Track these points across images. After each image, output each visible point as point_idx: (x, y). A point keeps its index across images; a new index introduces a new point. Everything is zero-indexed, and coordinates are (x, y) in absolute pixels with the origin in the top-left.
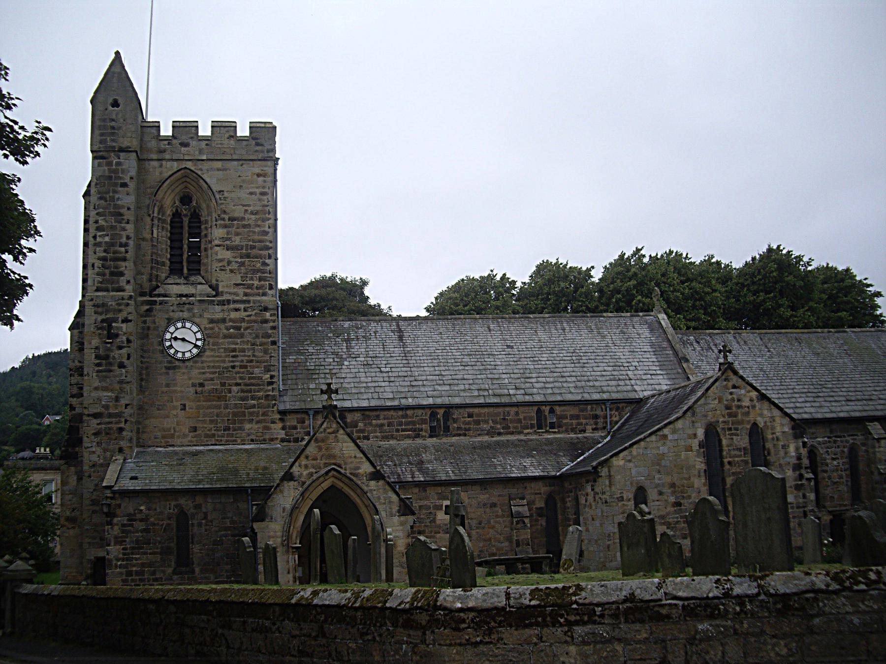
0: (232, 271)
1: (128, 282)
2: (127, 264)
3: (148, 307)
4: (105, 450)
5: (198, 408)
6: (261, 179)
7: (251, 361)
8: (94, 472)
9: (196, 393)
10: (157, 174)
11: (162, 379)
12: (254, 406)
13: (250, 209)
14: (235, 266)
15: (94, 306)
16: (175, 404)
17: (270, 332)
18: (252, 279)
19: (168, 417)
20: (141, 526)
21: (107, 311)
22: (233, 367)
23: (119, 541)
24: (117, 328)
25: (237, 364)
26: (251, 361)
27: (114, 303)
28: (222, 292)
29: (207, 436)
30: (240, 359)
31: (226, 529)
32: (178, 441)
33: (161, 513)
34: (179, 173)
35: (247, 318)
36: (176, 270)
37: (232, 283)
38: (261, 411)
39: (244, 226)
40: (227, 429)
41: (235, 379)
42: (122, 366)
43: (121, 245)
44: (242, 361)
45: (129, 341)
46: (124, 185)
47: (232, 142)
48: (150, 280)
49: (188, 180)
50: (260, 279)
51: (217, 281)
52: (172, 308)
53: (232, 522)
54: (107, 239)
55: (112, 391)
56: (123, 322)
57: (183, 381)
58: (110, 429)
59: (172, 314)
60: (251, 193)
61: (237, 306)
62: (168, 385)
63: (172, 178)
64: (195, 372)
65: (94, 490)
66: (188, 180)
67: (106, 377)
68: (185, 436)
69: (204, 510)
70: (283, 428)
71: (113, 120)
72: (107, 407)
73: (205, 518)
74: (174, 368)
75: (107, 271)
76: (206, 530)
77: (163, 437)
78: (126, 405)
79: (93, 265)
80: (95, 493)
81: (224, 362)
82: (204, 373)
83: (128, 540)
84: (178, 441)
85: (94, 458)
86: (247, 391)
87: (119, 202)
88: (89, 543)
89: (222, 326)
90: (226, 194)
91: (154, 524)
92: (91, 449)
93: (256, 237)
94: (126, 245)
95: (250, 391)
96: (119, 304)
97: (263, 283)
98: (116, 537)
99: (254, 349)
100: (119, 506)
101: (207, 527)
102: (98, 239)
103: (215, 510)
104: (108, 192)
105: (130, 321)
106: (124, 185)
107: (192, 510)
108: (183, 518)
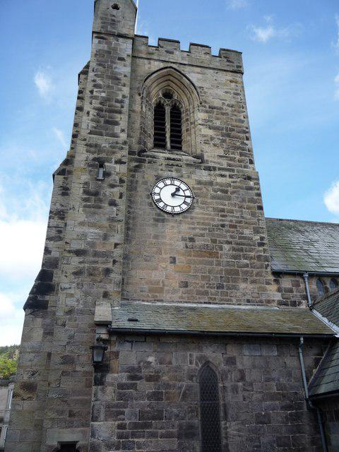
0: (215, 145)
1: (123, 131)
2: (122, 116)
3: (136, 164)
4: (87, 294)
5: (189, 262)
6: (233, 85)
7: (240, 222)
8: (70, 320)
9: (187, 247)
10: (147, 68)
11: (150, 231)
12: (247, 266)
13: (226, 103)
14: (218, 142)
15: (86, 145)
16: (164, 256)
17: (255, 198)
18: (233, 153)
19: (156, 269)
20: (146, 387)
21: (100, 151)
22: (223, 226)
23: (114, 412)
24: (110, 167)
25: (227, 223)
26: (240, 222)
27: (107, 146)
28: (207, 161)
29: (199, 293)
30: (229, 219)
31: (273, 397)
32: (168, 297)
33: (178, 368)
34: (166, 70)
35: (232, 184)
36: (159, 143)
37: (216, 154)
38: (255, 271)
39: (223, 114)
40: (220, 287)
41: (225, 237)
42: (113, 203)
43: (117, 101)
44: (231, 221)
45: (122, 181)
46: (122, 59)
47: (208, 56)
48: (139, 143)
49: (172, 78)
50: (241, 155)
51: (202, 151)
52: (161, 167)
53: (280, 387)
54: (103, 95)
55: (100, 227)
56: (116, 162)
57: (173, 235)
58: (94, 269)
59: (160, 172)
60: (226, 92)
61: (223, 173)
62: (156, 237)
63: (158, 73)
64: (184, 227)
65: (68, 343)
66: (172, 78)
67: (95, 213)
68: (174, 291)
69: (239, 366)
70: (279, 290)
71: (114, 16)
72: (92, 244)
73: (242, 378)
74: (163, 221)
75: (102, 120)
76: (244, 399)
77: (150, 291)
78: (116, 245)
79: (88, 113)
80: (68, 348)
81: (214, 220)
82: (193, 229)
83: (126, 410)
84: (168, 297)
85: (71, 302)
86: (238, 250)
87: (117, 70)
88: (52, 419)
89: (210, 188)
90: (206, 90)
91: (168, 386)
92: (69, 291)
93: (234, 123)
94: (121, 102)
95: (242, 250)
96: (114, 147)
97: (243, 157)
98: (108, 406)
99: (242, 211)
100: (117, 354)
101: (246, 394)
102: (95, 94)
103: (254, 367)
104: (107, 62)
105: (124, 163)
106: (122, 59)
107: (223, 366)
108: (209, 385)
